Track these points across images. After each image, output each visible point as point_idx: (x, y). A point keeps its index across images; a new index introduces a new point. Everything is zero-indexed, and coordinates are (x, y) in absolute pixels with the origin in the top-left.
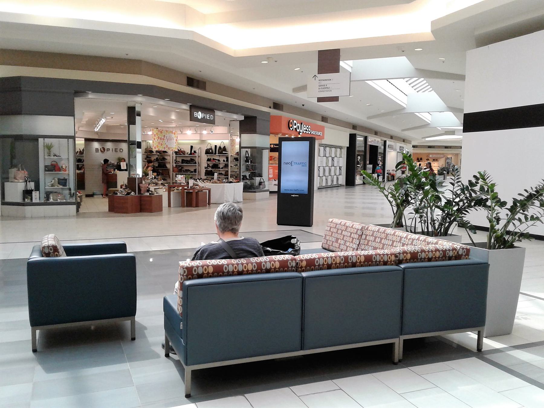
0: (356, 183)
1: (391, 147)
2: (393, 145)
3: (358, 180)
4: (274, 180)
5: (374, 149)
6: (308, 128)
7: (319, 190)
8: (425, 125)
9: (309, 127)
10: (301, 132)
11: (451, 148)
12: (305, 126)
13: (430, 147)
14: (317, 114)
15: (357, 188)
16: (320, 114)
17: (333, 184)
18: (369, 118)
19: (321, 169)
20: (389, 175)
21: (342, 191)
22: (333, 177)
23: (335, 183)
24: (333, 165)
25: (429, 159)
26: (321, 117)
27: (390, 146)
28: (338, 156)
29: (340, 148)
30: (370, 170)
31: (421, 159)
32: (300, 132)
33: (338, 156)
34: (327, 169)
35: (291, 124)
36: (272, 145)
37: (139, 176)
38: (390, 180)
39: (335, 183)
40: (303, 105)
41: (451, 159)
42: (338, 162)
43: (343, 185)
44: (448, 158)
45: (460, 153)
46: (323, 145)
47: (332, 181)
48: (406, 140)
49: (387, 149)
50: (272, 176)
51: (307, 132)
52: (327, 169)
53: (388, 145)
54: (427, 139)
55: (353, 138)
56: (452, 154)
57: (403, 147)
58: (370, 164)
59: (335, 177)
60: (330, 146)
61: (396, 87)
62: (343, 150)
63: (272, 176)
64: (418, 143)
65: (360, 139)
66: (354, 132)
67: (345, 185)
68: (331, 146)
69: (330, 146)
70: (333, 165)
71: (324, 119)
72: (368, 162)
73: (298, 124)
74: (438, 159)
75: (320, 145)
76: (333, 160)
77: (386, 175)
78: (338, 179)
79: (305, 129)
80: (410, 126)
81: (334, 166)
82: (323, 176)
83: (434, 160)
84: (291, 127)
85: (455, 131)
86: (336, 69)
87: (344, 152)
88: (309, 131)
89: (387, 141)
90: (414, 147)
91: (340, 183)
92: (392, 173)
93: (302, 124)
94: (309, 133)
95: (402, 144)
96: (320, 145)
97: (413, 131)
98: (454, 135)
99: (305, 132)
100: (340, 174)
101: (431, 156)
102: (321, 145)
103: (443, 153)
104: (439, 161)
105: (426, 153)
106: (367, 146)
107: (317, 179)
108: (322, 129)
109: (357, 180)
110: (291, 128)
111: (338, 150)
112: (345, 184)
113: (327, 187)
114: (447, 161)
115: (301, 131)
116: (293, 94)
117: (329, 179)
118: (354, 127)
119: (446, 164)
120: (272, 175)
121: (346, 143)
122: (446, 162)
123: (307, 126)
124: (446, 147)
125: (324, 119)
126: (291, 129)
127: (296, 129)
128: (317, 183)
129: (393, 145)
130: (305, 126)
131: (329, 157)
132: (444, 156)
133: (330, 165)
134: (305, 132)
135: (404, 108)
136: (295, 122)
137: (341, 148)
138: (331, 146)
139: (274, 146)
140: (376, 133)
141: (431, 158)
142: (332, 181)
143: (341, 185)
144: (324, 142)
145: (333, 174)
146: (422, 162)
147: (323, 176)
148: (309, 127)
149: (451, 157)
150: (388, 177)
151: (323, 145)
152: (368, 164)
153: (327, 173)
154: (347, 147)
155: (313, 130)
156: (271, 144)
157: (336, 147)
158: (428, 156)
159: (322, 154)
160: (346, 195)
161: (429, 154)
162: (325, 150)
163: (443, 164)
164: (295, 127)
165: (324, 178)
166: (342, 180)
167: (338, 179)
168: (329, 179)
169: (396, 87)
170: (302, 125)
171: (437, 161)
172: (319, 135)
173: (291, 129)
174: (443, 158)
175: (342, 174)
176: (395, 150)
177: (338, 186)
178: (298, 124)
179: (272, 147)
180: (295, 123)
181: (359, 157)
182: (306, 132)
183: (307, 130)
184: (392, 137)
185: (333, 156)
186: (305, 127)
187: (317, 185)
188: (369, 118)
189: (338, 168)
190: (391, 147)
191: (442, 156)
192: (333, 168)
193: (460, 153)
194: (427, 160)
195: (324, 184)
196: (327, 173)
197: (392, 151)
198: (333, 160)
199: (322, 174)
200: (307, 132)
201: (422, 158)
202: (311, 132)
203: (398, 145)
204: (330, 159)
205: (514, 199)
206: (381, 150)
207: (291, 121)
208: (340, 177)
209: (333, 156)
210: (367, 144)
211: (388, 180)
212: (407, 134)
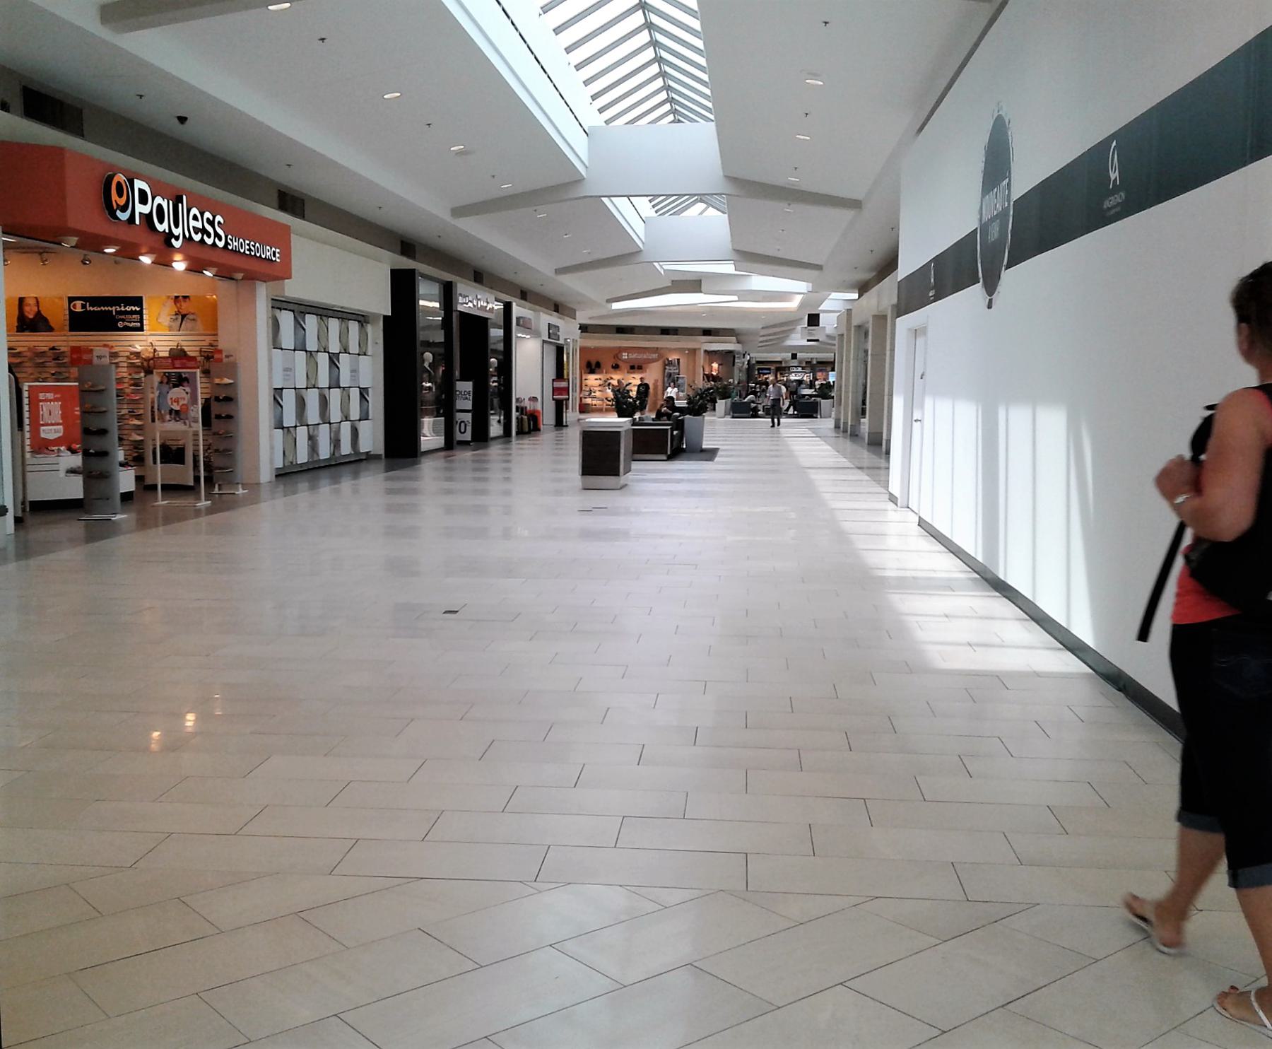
0: (424, 447)
1: (524, 324)
2: (529, 316)
3: (430, 434)
4: (69, 449)
5: (475, 325)
6: (211, 223)
7: (280, 478)
8: (628, 256)
9: (219, 218)
10: (177, 238)
11: (677, 335)
12: (194, 211)
13: (621, 330)
14: (259, 177)
15: (428, 467)
16: (271, 182)
17: (337, 455)
18: (458, 212)
19: (289, 400)
20: (522, 413)
21: (373, 482)
22: (339, 428)
23: (346, 448)
24: (334, 383)
25: (620, 363)
26: (276, 195)
27: (521, 322)
28: (354, 348)
29: (359, 322)
30: (467, 398)
31: (598, 365)
32: (170, 235)
33: (354, 348)
34: (312, 398)
35: (120, 195)
36: (79, 303)
37: (492, 414)
38: (526, 429)
39: (346, 448)
40: (182, 120)
41: (679, 363)
42: (354, 371)
43: (377, 457)
44: (670, 363)
45: (700, 349)
46: (291, 306)
47: (336, 443)
48: (562, 305)
49: (516, 333)
50: (56, 431)
51: (209, 241)
52: (312, 398)
53: (517, 318)
54: (617, 306)
55: (403, 286)
56: (681, 350)
57: (558, 327)
58: (463, 378)
59: (346, 429)
60: (320, 312)
61: (545, 72)
62: (369, 328)
63: (61, 434)
64: (590, 318)
65: (429, 303)
66: (406, 263)
67: (383, 456)
68: (324, 312)
69: (320, 312)
70: (334, 383)
71: (290, 201)
72: (457, 373)
73: (159, 200)
74: (644, 366)
75: (278, 304)
76: (333, 360)
77: (514, 414)
78: (355, 433)
79: (199, 225)
80: (584, 256)
81: (340, 387)
82: (296, 427)
83: (632, 367)
84: (124, 209)
85: (701, 281)
86: (796, 358)
87: (376, 334)
88: (217, 235)
89: (514, 304)
90: (584, 328)
91: (365, 445)
92: (528, 408)
93: (178, 200)
94: (221, 244)
95: (554, 319)
96: (278, 304)
97: (580, 274)
98: (701, 292)
99: (197, 237)
100: (365, 416)
101: (625, 356)
102: (279, 304)
103: (657, 348)
104: (648, 370)
105: (611, 349)
106: (455, 315)
107: (271, 436)
108: (281, 237)
109: (425, 436)
110: (119, 213)
111: (354, 327)
112: (380, 449)
113: (315, 470)
114: (667, 371)
115: (176, 232)
116: (104, 33)
117: (324, 433)
118: (407, 247)
119: (666, 379)
120: (61, 427)
121: (381, 304)
122: (664, 372)
123: (208, 215)
124: (665, 331)
125: (290, 201)
126: (124, 216)
127: (147, 218)
128: (272, 448)
129: (530, 319)
130: (194, 211)
131: (318, 351)
132: (660, 357)
133: (323, 381)
134: (197, 237)
135: (580, 180)
136: (139, 184)
137: (363, 319)
138: (325, 312)
139: (83, 306)
140: (479, 277)
141: (624, 361)
142: (336, 443)
143: (369, 457)
144: (293, 289)
145: (335, 415)
146: (602, 372)
147: (296, 427)
148: (219, 218)
149: (678, 360)
150: (520, 421)
151: (291, 306)
152: (459, 378)
153: (313, 415)
154: (385, 317)
155: (237, 236)
156: (71, 300)
157: (344, 316)
158: (617, 356)
159: (287, 338)
160: (390, 492)
161: (621, 350)
162: (299, 326)
163: (657, 378)
164: (141, 209)
165: (302, 433)
166: (372, 437)
167: (355, 433)
168: (324, 433)
169: (545, 72)
170: (182, 208)
171: (641, 371)
172: (268, 260)
173: (124, 216)
174: (655, 364)
175: (370, 418)
176: (536, 334)
177: (359, 461)
178: (159, 200)
179: (79, 309)
180: (142, 192)
181: (428, 356)
182: (202, 240)
183: (204, 231)
184: (524, 295)
185: (334, 347)
186: (195, 218)
187: (272, 461)
188: (458, 212)
189: (355, 394)
190: (524, 324)
191: (655, 356)
192: (335, 396)
193: (700, 349)
194: (613, 367)
195: (302, 457)
196: (313, 415)
197: (528, 337)
198: (333, 360)
199: (294, 418)
200: (209, 241)
201: (601, 361)
202: (227, 243)
203: (545, 319)
204: (323, 359)
205: (710, 454)
206: (496, 333)
207: (121, 177)
208: (364, 427)
209: (334, 347)
210: (454, 309)
211: (521, 432)
212: (572, 284)
